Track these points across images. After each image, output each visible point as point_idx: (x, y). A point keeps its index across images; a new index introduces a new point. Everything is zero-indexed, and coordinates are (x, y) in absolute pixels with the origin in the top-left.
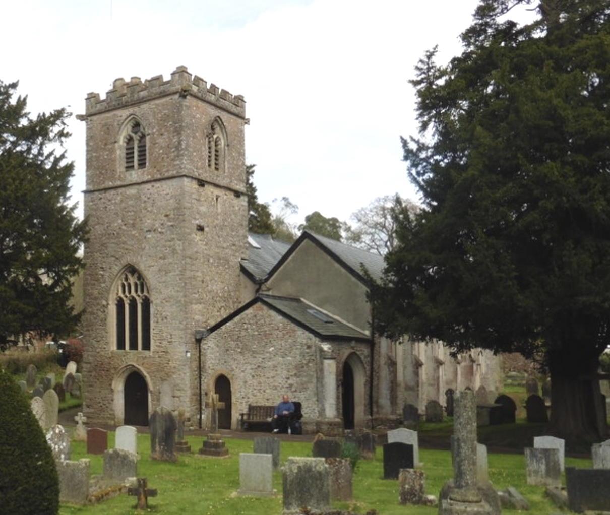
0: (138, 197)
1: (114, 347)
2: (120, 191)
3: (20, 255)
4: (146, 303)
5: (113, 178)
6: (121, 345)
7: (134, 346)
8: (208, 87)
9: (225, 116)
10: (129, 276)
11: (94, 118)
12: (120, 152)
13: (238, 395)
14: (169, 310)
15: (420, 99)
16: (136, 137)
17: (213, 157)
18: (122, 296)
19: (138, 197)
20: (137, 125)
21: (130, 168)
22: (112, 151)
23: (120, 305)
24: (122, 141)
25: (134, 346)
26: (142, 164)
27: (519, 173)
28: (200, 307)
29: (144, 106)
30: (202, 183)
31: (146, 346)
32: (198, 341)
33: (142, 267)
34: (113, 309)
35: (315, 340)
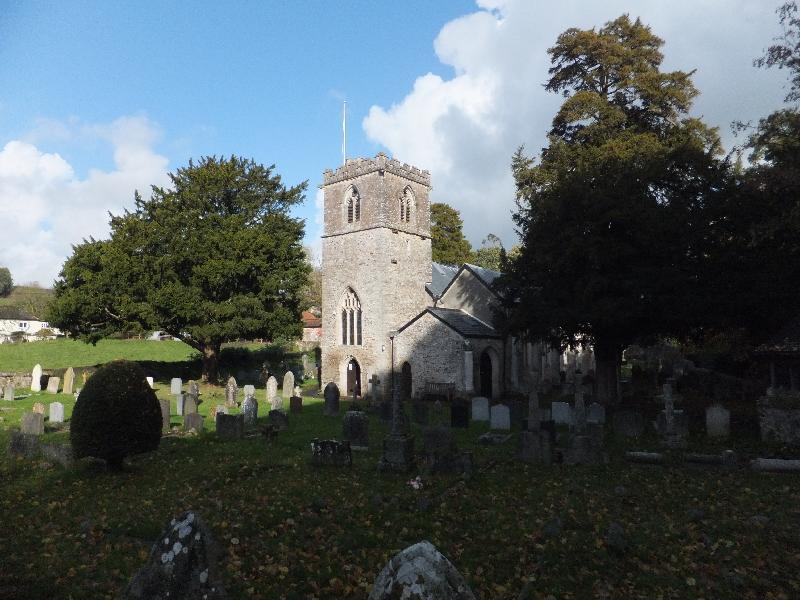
1: (341, 342)
3: (761, 133)
4: (360, 312)
5: (339, 228)
6: (345, 342)
7: (352, 342)
8: (402, 165)
9: (414, 184)
12: (344, 211)
13: (416, 375)
14: (373, 317)
15: (170, 187)
16: (355, 199)
17: (405, 214)
20: (355, 192)
21: (350, 220)
22: (339, 209)
23: (344, 314)
24: (346, 203)
25: (352, 342)
26: (358, 218)
27: (213, 590)
28: (393, 315)
30: (395, 231)
31: (360, 343)
32: (392, 338)
33: (356, 288)
34: (340, 317)
35: (461, 338)
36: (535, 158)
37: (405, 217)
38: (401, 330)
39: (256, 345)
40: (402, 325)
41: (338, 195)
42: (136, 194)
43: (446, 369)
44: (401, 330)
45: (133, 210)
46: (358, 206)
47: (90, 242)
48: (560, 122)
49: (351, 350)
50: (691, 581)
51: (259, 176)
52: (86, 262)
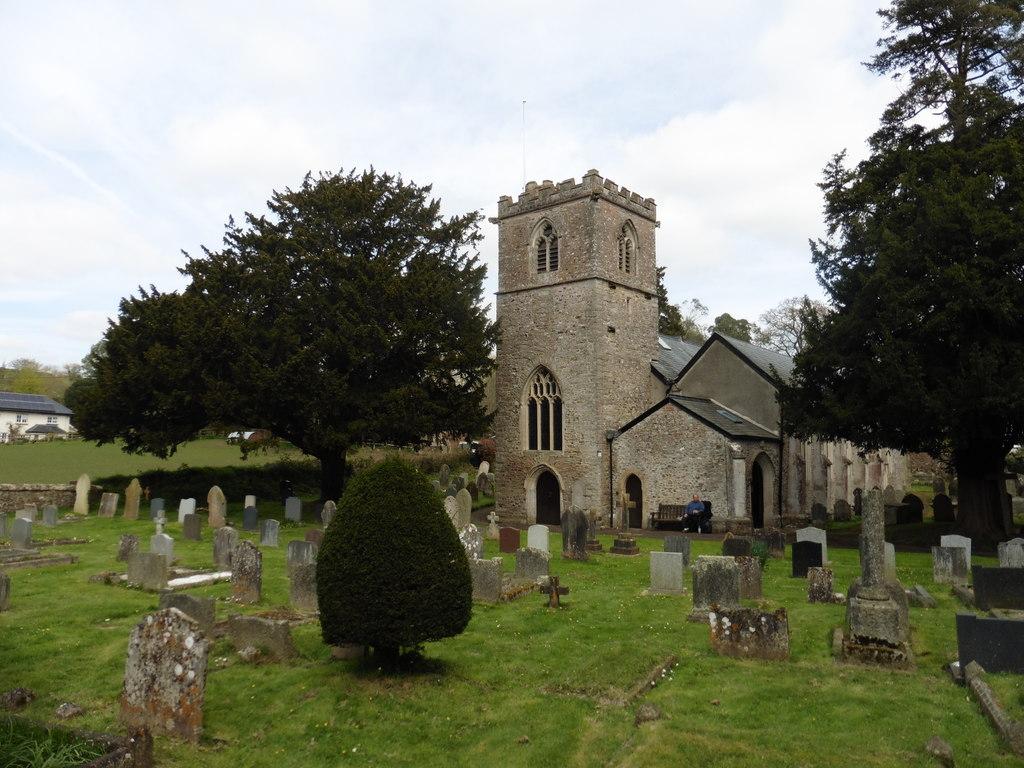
0: (550, 300)
1: (526, 447)
2: (532, 293)
4: (558, 404)
6: (533, 445)
7: (546, 446)
9: (636, 219)
10: (541, 377)
11: (507, 221)
12: (532, 255)
14: (581, 411)
16: (548, 240)
17: (624, 260)
18: (534, 396)
19: (550, 300)
20: (549, 228)
22: (525, 253)
23: (532, 405)
25: (546, 446)
26: (554, 267)
29: (556, 209)
30: (613, 285)
31: (558, 446)
32: (610, 441)
33: (553, 368)
34: (525, 410)
35: (725, 440)
36: (851, 164)
37: (624, 264)
38: (624, 429)
39: (11, 559)
40: (624, 423)
41: (521, 232)
42: (203, 247)
43: (701, 485)
44: (624, 429)
45: (219, 248)
46: (42, 562)
47: (150, 293)
48: (893, 114)
49: (544, 458)
50: (653, 683)
51: (407, 198)
52: (145, 324)
